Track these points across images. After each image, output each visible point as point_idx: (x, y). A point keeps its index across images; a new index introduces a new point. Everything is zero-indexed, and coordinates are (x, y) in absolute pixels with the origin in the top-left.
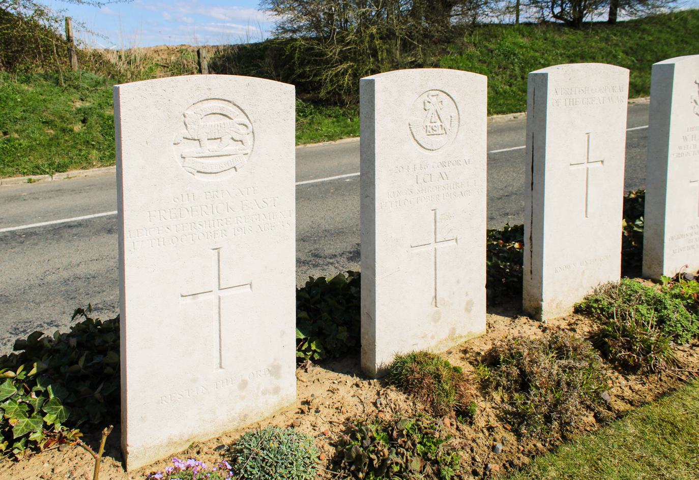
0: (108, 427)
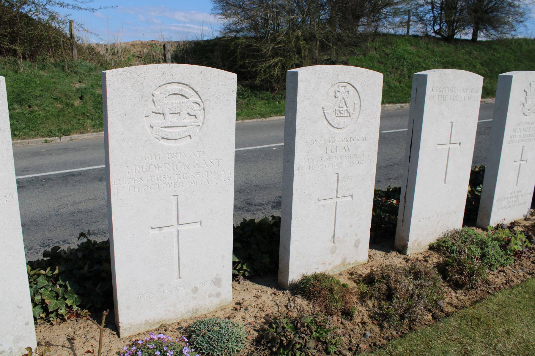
0: (106, 311)
